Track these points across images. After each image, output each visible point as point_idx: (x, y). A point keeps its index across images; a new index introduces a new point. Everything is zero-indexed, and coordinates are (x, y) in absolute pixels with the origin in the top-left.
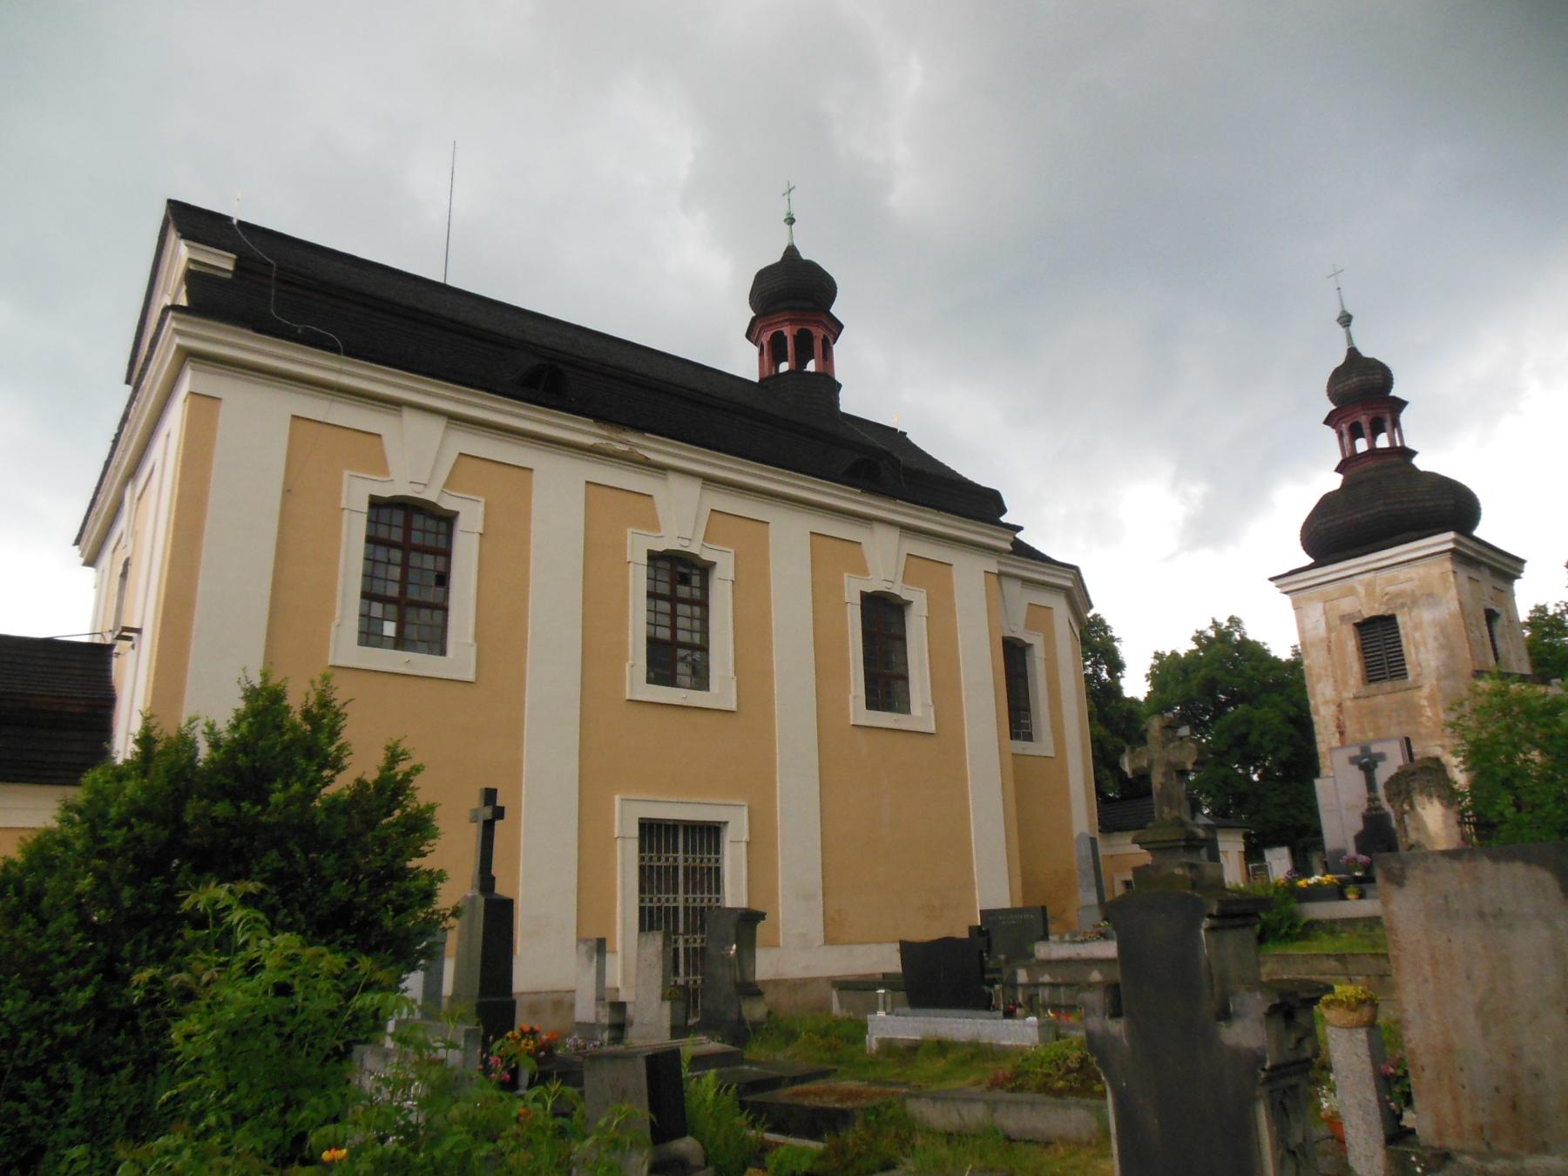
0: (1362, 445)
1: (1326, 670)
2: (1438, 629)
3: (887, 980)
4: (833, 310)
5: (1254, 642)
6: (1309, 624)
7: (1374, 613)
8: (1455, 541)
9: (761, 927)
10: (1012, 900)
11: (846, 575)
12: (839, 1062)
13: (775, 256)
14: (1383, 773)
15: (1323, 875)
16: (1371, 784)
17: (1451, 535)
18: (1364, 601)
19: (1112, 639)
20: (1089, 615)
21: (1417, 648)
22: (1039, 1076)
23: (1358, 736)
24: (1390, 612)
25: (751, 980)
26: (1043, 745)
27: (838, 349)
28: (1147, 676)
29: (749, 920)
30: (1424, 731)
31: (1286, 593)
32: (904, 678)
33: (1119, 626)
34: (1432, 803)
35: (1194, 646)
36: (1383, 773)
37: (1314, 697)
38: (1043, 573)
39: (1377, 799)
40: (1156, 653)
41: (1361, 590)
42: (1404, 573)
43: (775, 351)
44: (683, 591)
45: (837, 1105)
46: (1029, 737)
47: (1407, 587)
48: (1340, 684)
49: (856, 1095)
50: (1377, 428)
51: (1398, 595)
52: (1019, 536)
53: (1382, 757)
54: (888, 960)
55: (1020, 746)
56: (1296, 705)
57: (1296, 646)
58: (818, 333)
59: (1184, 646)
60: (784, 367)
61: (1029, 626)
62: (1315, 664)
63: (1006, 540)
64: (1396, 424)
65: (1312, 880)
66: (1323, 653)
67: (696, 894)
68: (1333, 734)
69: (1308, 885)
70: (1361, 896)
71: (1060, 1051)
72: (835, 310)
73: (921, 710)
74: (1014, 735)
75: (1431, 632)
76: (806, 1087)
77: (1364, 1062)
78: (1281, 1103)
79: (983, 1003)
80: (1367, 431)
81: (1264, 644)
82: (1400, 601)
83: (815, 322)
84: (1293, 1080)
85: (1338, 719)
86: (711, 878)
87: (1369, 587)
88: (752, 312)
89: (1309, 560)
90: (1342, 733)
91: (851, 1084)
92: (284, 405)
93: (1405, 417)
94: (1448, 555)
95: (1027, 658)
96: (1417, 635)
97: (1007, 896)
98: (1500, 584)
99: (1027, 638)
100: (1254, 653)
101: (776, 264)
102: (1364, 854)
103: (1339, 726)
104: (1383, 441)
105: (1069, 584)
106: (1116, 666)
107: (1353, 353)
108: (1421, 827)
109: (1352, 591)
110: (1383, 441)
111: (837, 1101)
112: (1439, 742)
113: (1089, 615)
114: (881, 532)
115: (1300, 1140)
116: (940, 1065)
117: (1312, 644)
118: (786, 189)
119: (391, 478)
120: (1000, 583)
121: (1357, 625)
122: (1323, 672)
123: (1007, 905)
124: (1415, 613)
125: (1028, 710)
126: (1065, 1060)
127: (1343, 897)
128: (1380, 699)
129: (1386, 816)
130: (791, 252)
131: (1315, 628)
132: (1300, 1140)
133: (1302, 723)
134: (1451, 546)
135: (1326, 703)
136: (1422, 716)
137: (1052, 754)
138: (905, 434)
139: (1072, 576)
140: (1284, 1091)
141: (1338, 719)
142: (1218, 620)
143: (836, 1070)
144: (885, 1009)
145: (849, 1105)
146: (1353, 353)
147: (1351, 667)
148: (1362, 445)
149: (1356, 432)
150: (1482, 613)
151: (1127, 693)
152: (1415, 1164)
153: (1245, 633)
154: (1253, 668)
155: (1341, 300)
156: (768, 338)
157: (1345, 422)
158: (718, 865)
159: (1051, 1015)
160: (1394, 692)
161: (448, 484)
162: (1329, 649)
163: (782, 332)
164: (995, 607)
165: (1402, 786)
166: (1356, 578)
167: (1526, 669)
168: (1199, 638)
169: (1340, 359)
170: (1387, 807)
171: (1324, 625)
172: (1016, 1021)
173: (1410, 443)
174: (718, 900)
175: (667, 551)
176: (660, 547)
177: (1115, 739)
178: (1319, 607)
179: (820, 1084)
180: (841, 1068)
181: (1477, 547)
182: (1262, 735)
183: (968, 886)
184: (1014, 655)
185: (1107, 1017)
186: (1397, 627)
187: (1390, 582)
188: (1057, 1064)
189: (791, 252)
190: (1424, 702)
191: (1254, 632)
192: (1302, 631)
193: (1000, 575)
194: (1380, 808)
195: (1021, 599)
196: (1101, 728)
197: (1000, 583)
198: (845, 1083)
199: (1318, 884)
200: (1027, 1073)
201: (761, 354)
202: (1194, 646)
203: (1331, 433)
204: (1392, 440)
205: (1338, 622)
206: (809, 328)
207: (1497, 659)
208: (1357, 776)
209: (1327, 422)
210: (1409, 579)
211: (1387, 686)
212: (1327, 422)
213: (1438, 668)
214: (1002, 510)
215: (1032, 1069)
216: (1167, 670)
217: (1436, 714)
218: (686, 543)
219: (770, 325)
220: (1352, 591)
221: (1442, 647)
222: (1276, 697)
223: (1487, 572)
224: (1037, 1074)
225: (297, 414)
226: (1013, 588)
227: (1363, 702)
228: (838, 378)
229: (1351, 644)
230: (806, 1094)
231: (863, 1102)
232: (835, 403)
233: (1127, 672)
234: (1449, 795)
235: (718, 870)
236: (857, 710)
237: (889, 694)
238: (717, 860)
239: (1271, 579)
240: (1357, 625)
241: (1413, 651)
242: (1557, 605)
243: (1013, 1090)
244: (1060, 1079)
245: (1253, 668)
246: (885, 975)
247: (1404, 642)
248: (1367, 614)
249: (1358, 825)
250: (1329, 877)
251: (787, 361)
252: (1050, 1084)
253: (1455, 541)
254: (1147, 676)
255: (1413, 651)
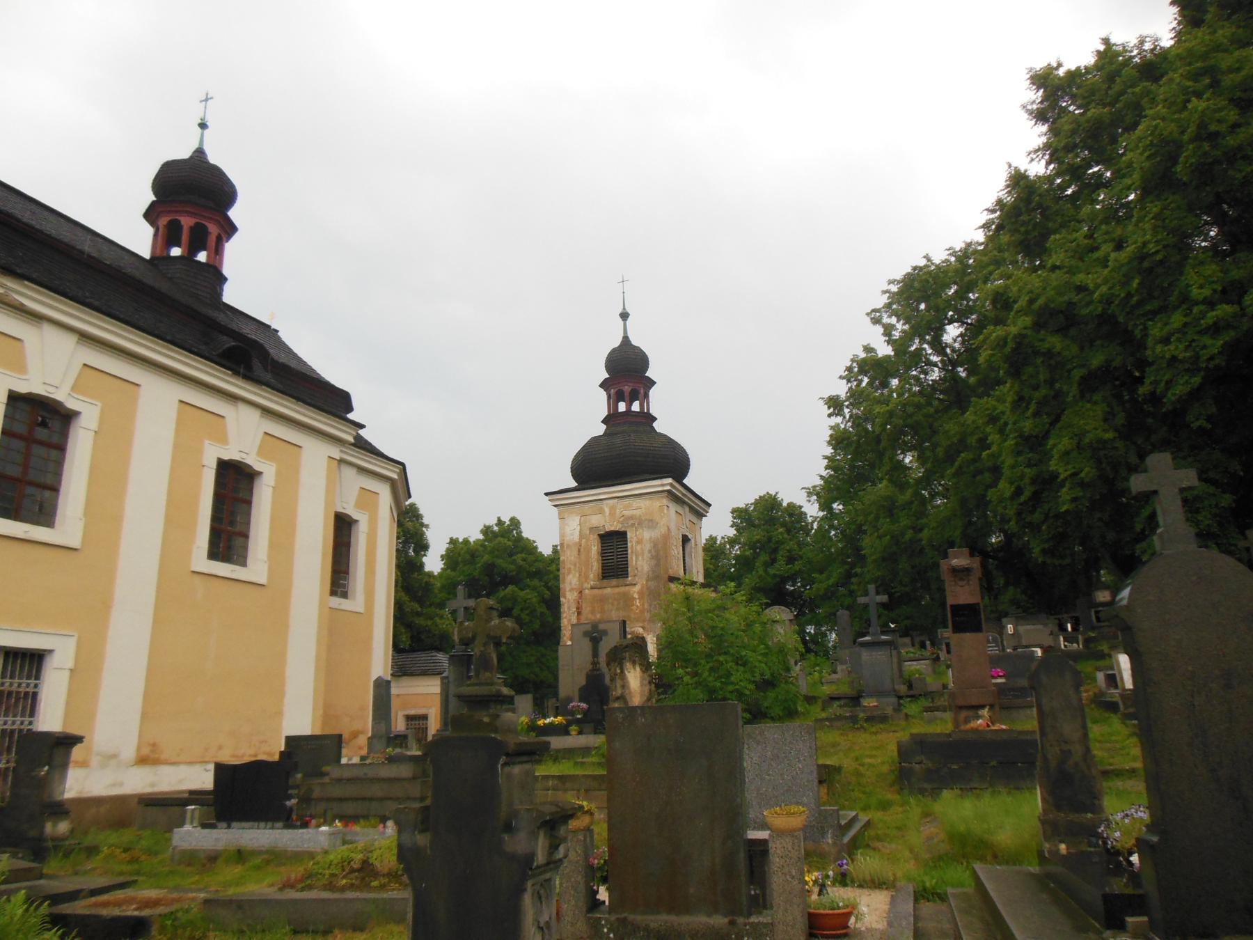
0: (622, 407)
1: (575, 565)
2: (652, 545)
3: (195, 797)
4: (600, 429)
5: (527, 539)
6: (568, 530)
7: (612, 529)
8: (671, 485)
9: (77, 752)
10: (312, 729)
11: (207, 442)
12: (138, 873)
13: (184, 153)
14: (606, 646)
15: (555, 717)
16: (595, 654)
17: (670, 480)
18: (607, 518)
19: (422, 525)
20: (407, 503)
21: (637, 558)
22: (327, 876)
23: (590, 616)
24: (623, 529)
25: (59, 798)
26: (356, 604)
27: (232, 249)
28: (442, 556)
29: (66, 742)
30: (633, 616)
31: (555, 506)
32: (245, 536)
33: (428, 515)
34: (635, 669)
35: (481, 537)
36: (606, 646)
37: (564, 582)
38: (376, 465)
39: (598, 663)
40: (451, 539)
41: (607, 510)
42: (636, 503)
43: (168, 236)
44: (41, 433)
45: (136, 913)
46: (345, 595)
47: (638, 512)
48: (584, 577)
49: (155, 903)
50: (634, 396)
51: (631, 517)
52: (362, 432)
53: (605, 632)
54: (204, 779)
55: (336, 602)
56: (549, 589)
57: (556, 546)
58: (213, 230)
59: (475, 535)
60: (176, 252)
61: (360, 505)
62: (568, 557)
63: (350, 434)
64: (646, 396)
65: (548, 721)
66: (575, 553)
67: (7, 717)
68: (574, 613)
69: (544, 724)
70: (580, 733)
71: (347, 854)
72: (233, 214)
73: (257, 567)
74: (333, 593)
75: (648, 546)
76: (105, 897)
77: (579, 855)
78: (538, 893)
79: (287, 819)
80: (627, 398)
81: (534, 542)
82: (631, 522)
83: (211, 219)
84: (547, 876)
85: (579, 602)
86: (30, 702)
87: (612, 509)
88: (151, 193)
89: (574, 484)
90: (579, 613)
91: (152, 893)
92: (177, 392)
93: (653, 393)
94: (666, 494)
95: (353, 532)
96: (639, 548)
97: (310, 727)
98: (694, 519)
99: (355, 516)
100: (528, 548)
101: (184, 160)
102: (584, 703)
103: (578, 608)
104: (636, 407)
105: (395, 476)
106: (423, 547)
107: (626, 339)
108: (625, 686)
109: (601, 511)
110: (636, 407)
111: (136, 909)
112: (641, 625)
113: (407, 503)
114: (244, 410)
115: (548, 919)
116: (238, 870)
117: (568, 546)
118: (204, 98)
119: (24, 377)
120: (339, 468)
121: (601, 536)
122: (572, 567)
123: (308, 732)
124: (640, 531)
125: (347, 572)
126: (349, 863)
127: (567, 733)
128: (609, 590)
129: (602, 676)
130: (200, 153)
131: (572, 535)
132: (548, 919)
133: (553, 603)
134: (668, 488)
135: (572, 590)
136: (633, 605)
137: (362, 610)
138: (277, 331)
139: (398, 471)
140: (542, 885)
141: (579, 602)
142: (502, 519)
143: (136, 881)
144: (192, 823)
145: (146, 913)
146: (626, 339)
147: (592, 566)
148: (622, 407)
149: (620, 397)
150: (681, 537)
151: (427, 568)
152: (603, 926)
153: (521, 532)
154: (524, 560)
155: (205, 112)
156: (165, 223)
157: (614, 388)
158: (36, 690)
159: (339, 824)
160: (618, 586)
161: (75, 388)
162: (579, 551)
163: (179, 221)
164: (331, 488)
165: (617, 656)
166: (605, 502)
167: (701, 579)
168: (487, 531)
169: (617, 343)
170: (604, 669)
171: (578, 533)
172: (310, 830)
173: (653, 412)
174: (31, 723)
175: (30, 394)
176: (23, 388)
177: (412, 604)
178: (577, 519)
179: (120, 894)
180: (141, 878)
181: (684, 491)
182: (522, 610)
183: (279, 714)
184: (343, 526)
185: (416, 832)
186: (627, 541)
187: (627, 508)
188: (343, 866)
189: (200, 153)
190: (636, 596)
191: (527, 532)
192: (562, 535)
193: (341, 461)
194: (599, 670)
195: (353, 483)
196: (403, 594)
197: (339, 468)
198: (144, 892)
199: (551, 724)
200: (317, 873)
201: (156, 235)
202: (481, 537)
203: (603, 395)
204: (642, 406)
205: (588, 532)
206: (206, 224)
207: (685, 570)
208: (586, 645)
209: (602, 385)
210: (639, 508)
211: (614, 582)
212: (602, 385)
213: (648, 572)
214: (350, 408)
215: (320, 871)
216: (458, 554)
217: (643, 605)
218: (244, 456)
219: (169, 212)
220: (601, 511)
221: (652, 557)
222: (536, 582)
223: (687, 509)
224: (324, 875)
225: (87, 363)
226: (349, 473)
227: (596, 591)
228: (226, 271)
229: (595, 549)
230: (105, 904)
231: (161, 910)
232: (219, 295)
233: (430, 552)
234: (646, 666)
235: (35, 695)
236: (200, 559)
237: (229, 548)
238: (36, 686)
239: (547, 494)
240: (601, 536)
241: (634, 558)
242: (723, 538)
243: (302, 890)
244: (344, 877)
245: (524, 560)
246: (191, 792)
247: (629, 551)
248: (609, 528)
249: (582, 681)
250: (560, 718)
251: (179, 246)
252: (334, 883)
253: (671, 485)
254: (442, 556)
255: (634, 558)
